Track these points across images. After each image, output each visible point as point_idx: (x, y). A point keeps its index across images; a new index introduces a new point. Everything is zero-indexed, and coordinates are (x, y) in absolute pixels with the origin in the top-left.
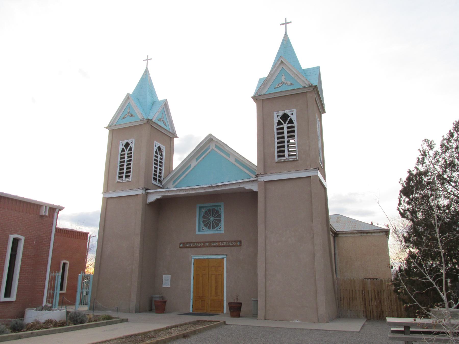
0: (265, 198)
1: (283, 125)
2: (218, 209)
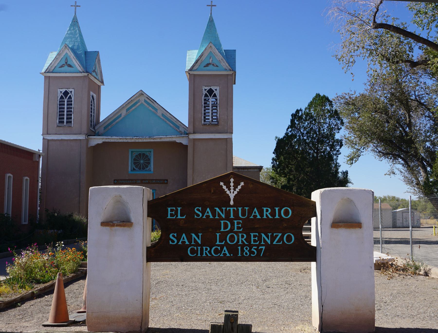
0: (194, 151)
1: (64, 99)
2: (147, 154)
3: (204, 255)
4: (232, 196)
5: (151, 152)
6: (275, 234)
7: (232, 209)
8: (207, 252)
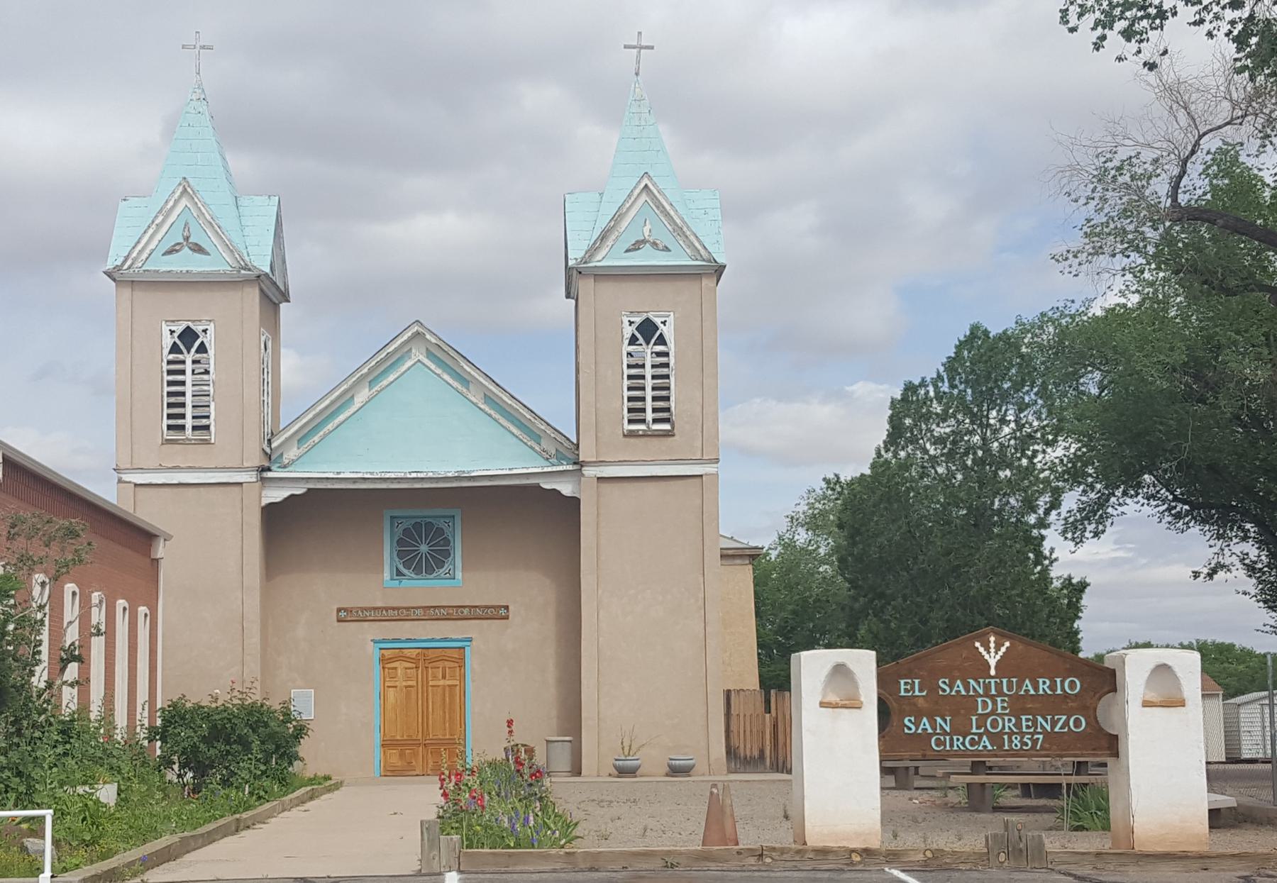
2: (441, 524)
3: (955, 748)
4: (993, 663)
5: (454, 517)
6: (1056, 717)
7: (993, 681)
8: (959, 743)
